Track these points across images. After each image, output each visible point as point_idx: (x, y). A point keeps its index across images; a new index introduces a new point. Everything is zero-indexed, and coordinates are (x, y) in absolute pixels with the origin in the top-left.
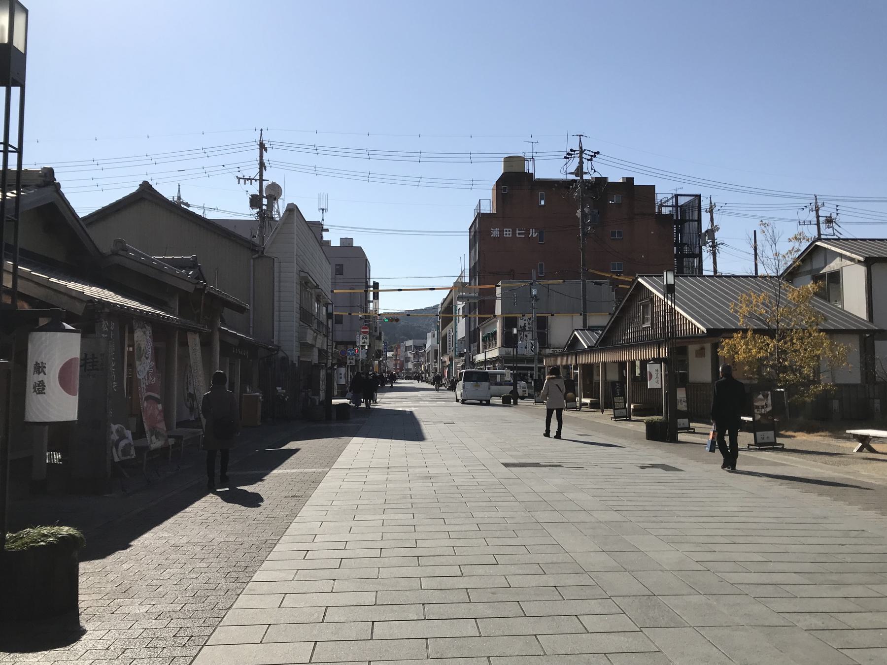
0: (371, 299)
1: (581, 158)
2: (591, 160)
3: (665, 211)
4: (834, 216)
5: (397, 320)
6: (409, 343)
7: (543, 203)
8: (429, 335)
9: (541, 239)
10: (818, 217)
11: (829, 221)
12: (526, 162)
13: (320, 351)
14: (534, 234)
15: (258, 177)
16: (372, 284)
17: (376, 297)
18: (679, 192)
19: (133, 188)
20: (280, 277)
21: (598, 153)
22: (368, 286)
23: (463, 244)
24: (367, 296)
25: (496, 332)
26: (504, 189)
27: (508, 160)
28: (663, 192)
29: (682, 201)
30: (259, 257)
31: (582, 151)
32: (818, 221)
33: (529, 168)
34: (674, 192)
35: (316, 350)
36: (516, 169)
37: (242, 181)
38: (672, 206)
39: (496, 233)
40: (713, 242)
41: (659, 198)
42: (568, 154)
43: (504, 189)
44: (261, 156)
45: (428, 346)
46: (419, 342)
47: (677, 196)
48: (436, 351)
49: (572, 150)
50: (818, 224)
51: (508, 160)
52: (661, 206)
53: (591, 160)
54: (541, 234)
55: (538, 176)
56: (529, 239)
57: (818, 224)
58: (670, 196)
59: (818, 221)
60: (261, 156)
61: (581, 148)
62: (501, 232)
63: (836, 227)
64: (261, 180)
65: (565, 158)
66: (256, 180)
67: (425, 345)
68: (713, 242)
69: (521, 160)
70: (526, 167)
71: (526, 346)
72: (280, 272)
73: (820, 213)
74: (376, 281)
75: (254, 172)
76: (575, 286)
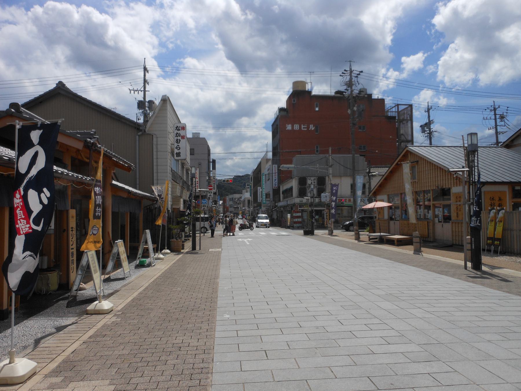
0: (211, 169)
1: (351, 75)
2: (357, 77)
4: (505, 114)
7: (317, 109)
10: (495, 114)
11: (502, 117)
12: (307, 85)
13: (185, 201)
14: (312, 127)
15: (143, 89)
16: (211, 161)
17: (214, 168)
18: (399, 103)
19: (52, 86)
20: (157, 169)
21: (362, 72)
22: (209, 162)
24: (209, 168)
25: (291, 189)
29: (401, 108)
30: (142, 134)
31: (351, 72)
32: (495, 117)
34: (396, 102)
35: (182, 200)
36: (300, 88)
37: (132, 92)
38: (395, 112)
39: (289, 127)
40: (430, 130)
42: (343, 73)
44: (145, 75)
47: (398, 105)
49: (345, 70)
50: (495, 119)
51: (295, 84)
53: (357, 77)
54: (316, 130)
56: (308, 131)
57: (495, 119)
58: (394, 105)
59: (495, 117)
60: (145, 75)
61: (351, 69)
62: (293, 127)
63: (506, 121)
64: (145, 91)
65: (341, 76)
66: (141, 91)
68: (430, 130)
69: (304, 83)
70: (307, 87)
72: (157, 166)
73: (497, 112)
74: (214, 158)
75: (140, 86)
76: (346, 158)
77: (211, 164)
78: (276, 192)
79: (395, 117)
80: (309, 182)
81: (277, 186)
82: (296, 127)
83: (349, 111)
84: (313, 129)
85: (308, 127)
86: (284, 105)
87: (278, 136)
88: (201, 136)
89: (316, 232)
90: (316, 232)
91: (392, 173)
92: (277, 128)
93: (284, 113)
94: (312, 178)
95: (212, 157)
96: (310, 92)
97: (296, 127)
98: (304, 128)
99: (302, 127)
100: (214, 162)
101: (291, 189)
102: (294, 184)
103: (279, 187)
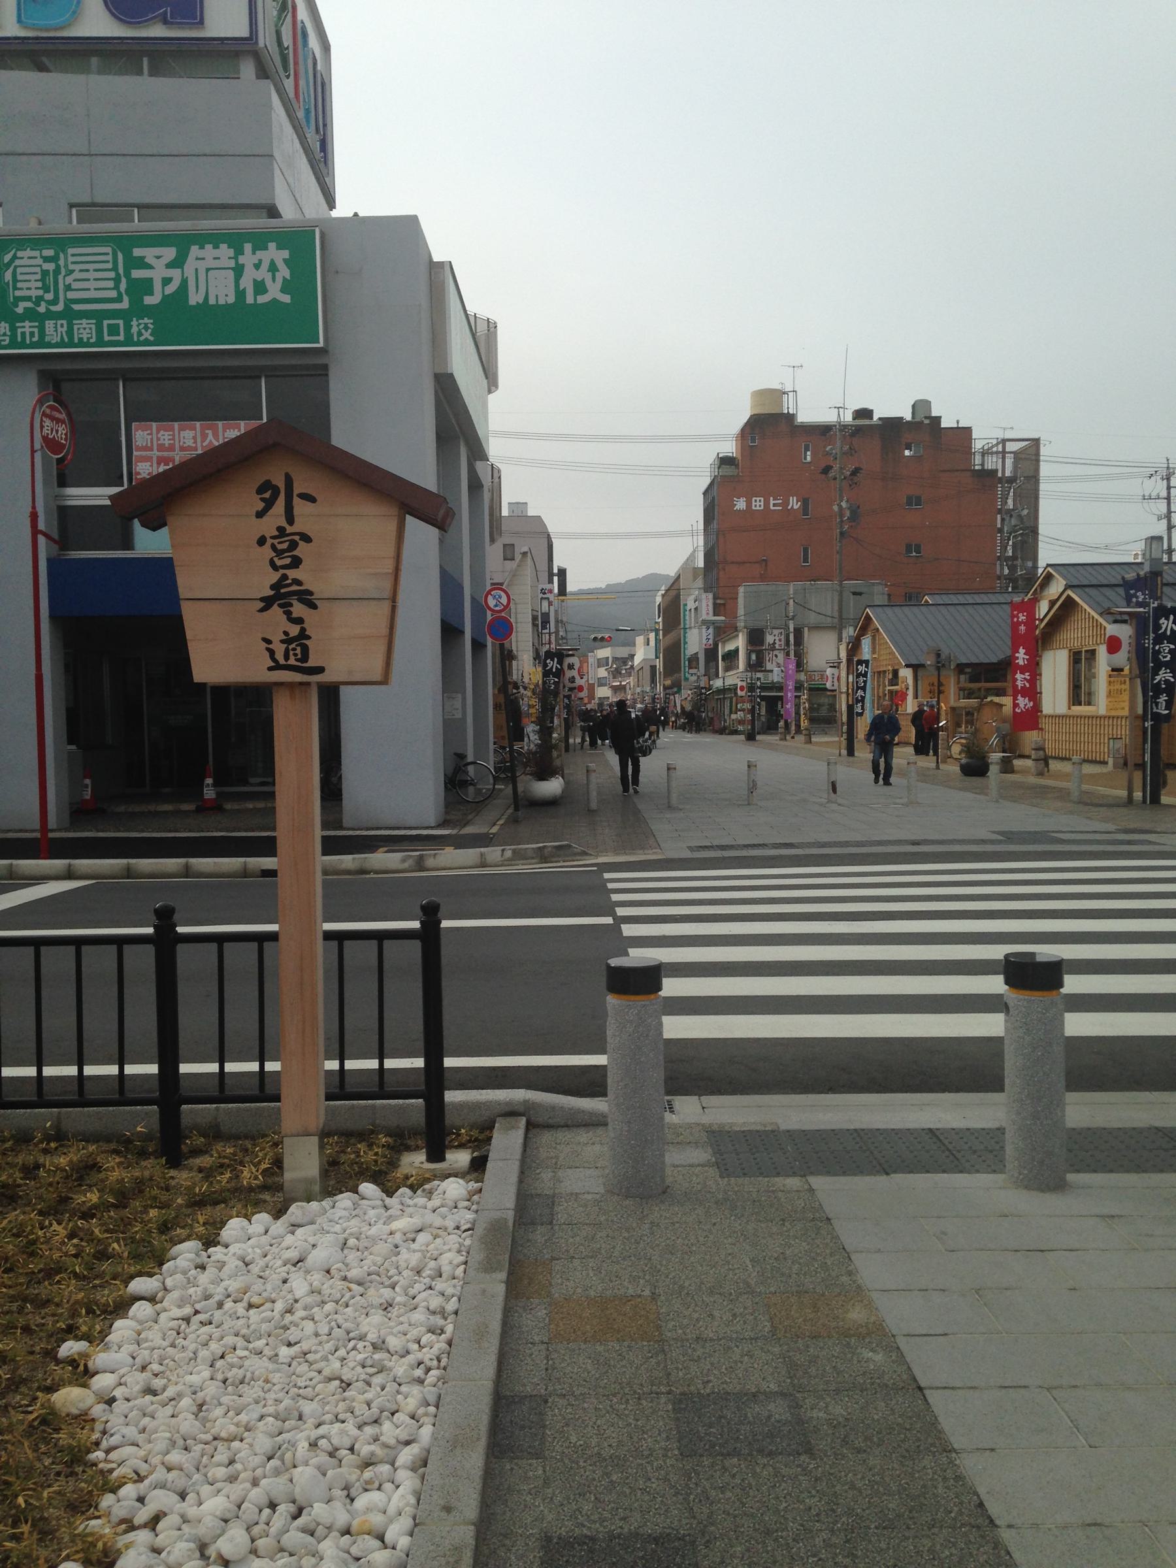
3: (991, 463)
5: (325, 163)
6: (604, 653)
8: (640, 640)
9: (805, 512)
16: (555, 571)
23: (691, 514)
25: (737, 650)
26: (753, 440)
27: (762, 395)
28: (982, 437)
33: (788, 406)
34: (1001, 436)
39: (741, 504)
41: (978, 445)
43: (753, 440)
45: (637, 660)
46: (623, 652)
48: (653, 668)
52: (985, 453)
54: (805, 502)
55: (803, 417)
56: (787, 511)
58: (995, 442)
62: (749, 504)
67: (632, 656)
69: (778, 395)
71: (776, 670)
74: (563, 566)
77: (556, 579)
78: (711, 654)
79: (997, 471)
80: (769, 639)
81: (711, 642)
82: (758, 504)
83: (836, 508)
84: (796, 507)
85: (786, 503)
86: (729, 448)
87: (715, 525)
88: (531, 512)
89: (758, 737)
90: (758, 737)
91: (874, 637)
92: (713, 507)
93: (728, 470)
94: (776, 632)
95: (557, 563)
96: (790, 417)
97: (758, 504)
98: (774, 505)
99: (772, 502)
100: (562, 573)
101: (737, 650)
102: (740, 642)
103: (716, 645)
